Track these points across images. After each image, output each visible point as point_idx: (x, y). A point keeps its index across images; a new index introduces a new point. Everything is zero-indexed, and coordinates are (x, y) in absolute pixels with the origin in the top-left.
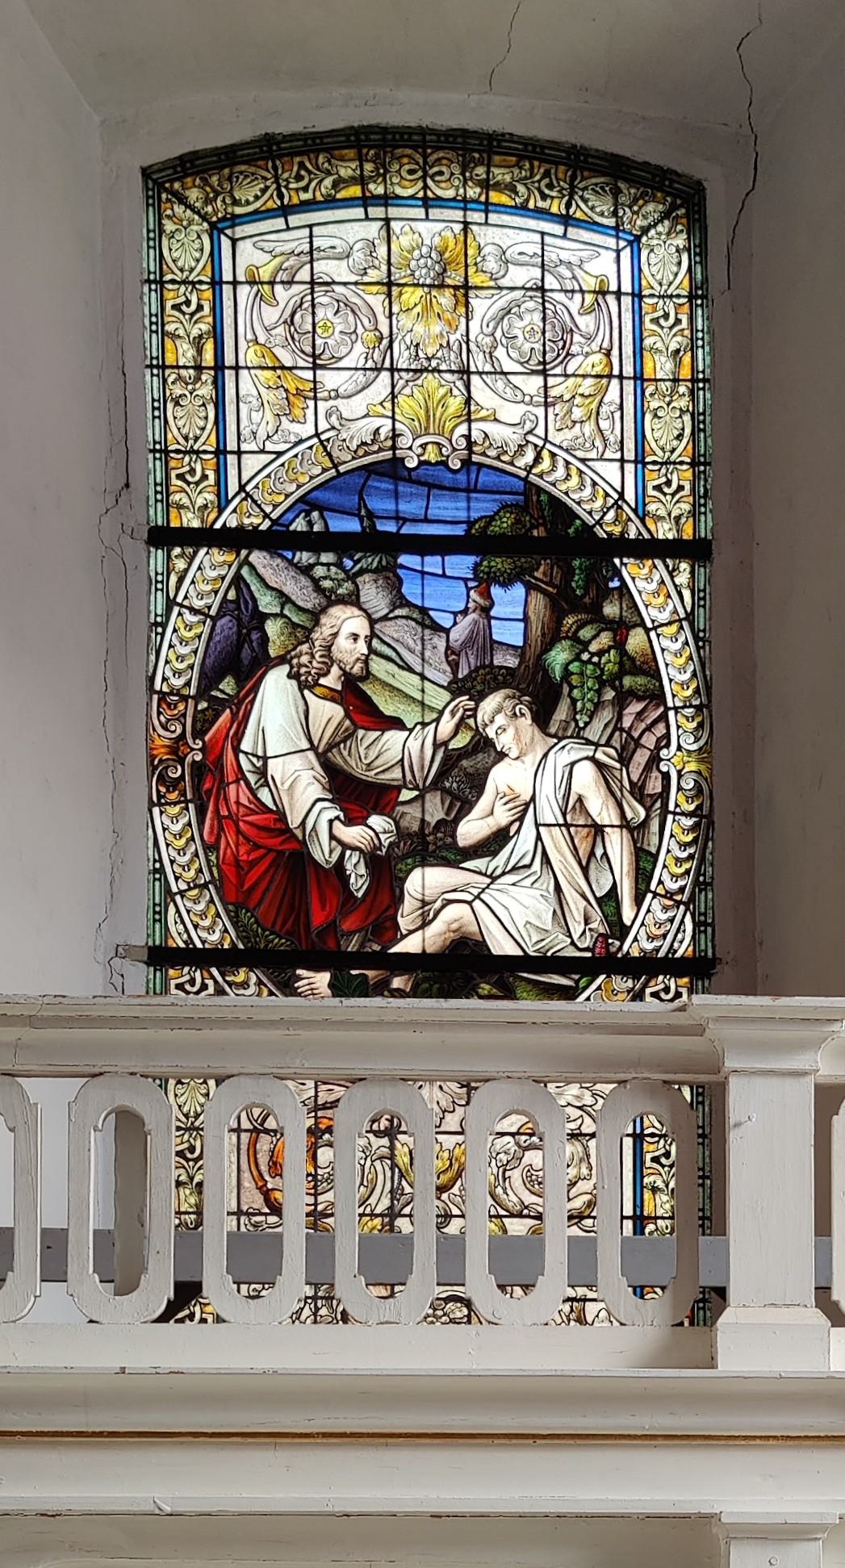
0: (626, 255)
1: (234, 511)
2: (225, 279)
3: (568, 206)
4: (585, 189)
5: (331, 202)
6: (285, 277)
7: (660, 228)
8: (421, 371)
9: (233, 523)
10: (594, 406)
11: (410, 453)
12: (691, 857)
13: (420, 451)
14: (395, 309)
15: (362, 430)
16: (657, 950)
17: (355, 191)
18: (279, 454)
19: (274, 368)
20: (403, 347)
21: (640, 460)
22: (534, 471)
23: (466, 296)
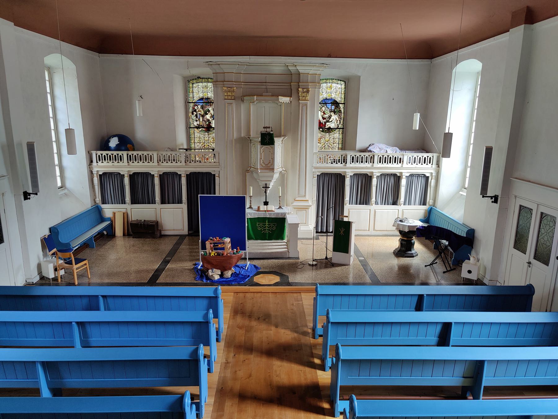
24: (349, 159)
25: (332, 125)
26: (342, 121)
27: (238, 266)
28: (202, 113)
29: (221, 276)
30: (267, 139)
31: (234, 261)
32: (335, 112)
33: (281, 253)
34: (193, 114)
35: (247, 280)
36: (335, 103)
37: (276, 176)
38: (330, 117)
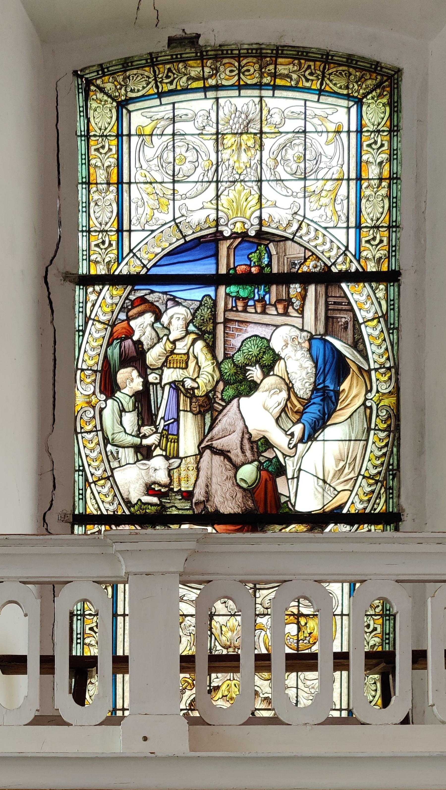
0: (354, 110)
1: (127, 264)
2: (124, 181)
3: (321, 84)
4: (330, 74)
5: (186, 90)
6: (159, 132)
7: (374, 93)
8: (234, 182)
9: (125, 272)
10: (333, 196)
11: (227, 228)
12: (384, 454)
13: (232, 227)
14: (220, 148)
15: (198, 217)
16: (365, 509)
17: (200, 84)
18: (153, 231)
19: (151, 183)
20: (224, 168)
21: (359, 227)
22: (298, 234)
23: (261, 138)
28: (203, 373)
34: (109, 387)
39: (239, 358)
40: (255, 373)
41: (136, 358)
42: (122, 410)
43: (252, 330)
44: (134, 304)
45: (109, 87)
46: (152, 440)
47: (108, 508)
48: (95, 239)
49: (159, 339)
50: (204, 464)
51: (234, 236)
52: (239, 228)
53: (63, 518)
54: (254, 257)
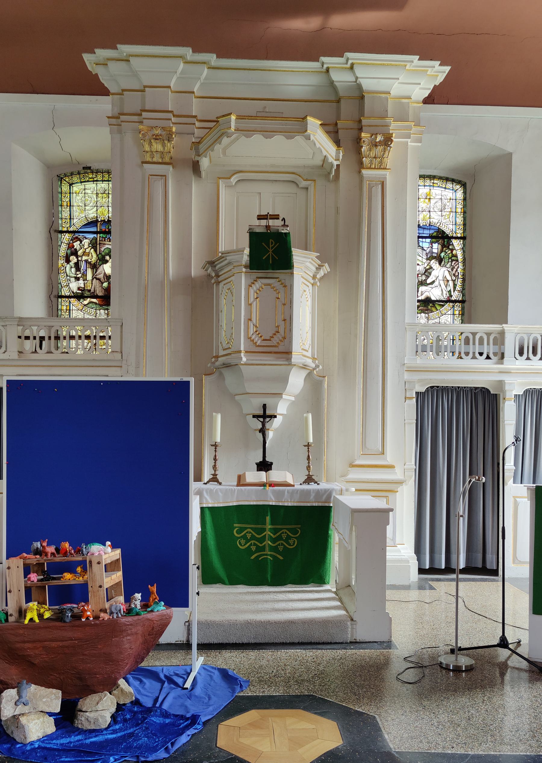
5: (88, 181)
15: (91, 216)
17: (92, 180)
24: (510, 347)
25: (435, 293)
26: (459, 283)
27: (153, 675)
28: (94, 258)
29: (66, 717)
30: (270, 252)
31: (130, 644)
32: (440, 261)
33: (325, 623)
34: (68, 261)
35: (184, 739)
36: (441, 237)
37: (296, 381)
38: (428, 272)
39: (103, 254)
40: (107, 258)
41: (75, 253)
42: (71, 267)
43: (107, 246)
44: (74, 239)
45: (67, 180)
46: (79, 276)
47: (68, 294)
48: (64, 221)
49: (81, 248)
50: (93, 282)
51: (101, 221)
52: (103, 219)
53: (55, 297)
54: (107, 227)
